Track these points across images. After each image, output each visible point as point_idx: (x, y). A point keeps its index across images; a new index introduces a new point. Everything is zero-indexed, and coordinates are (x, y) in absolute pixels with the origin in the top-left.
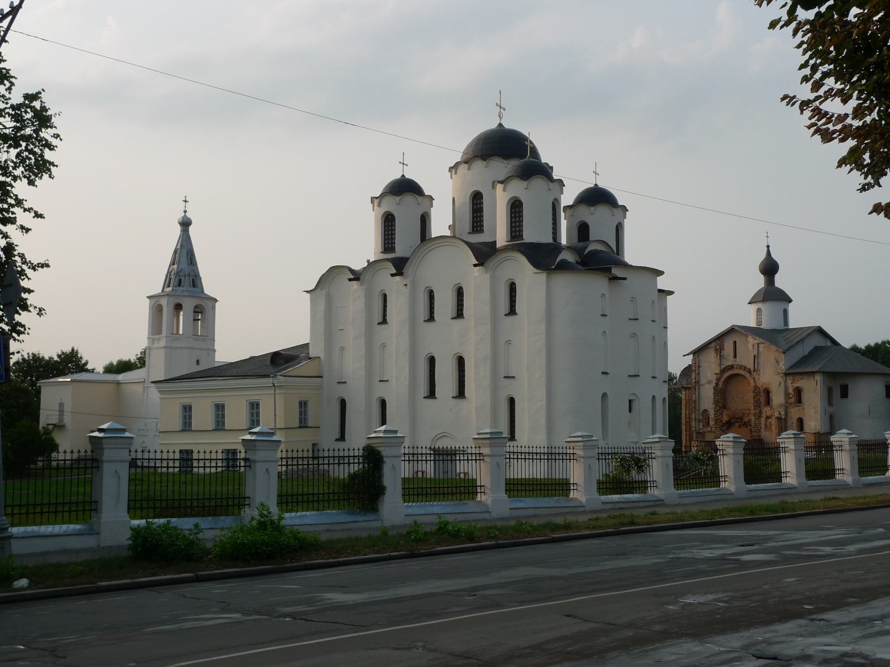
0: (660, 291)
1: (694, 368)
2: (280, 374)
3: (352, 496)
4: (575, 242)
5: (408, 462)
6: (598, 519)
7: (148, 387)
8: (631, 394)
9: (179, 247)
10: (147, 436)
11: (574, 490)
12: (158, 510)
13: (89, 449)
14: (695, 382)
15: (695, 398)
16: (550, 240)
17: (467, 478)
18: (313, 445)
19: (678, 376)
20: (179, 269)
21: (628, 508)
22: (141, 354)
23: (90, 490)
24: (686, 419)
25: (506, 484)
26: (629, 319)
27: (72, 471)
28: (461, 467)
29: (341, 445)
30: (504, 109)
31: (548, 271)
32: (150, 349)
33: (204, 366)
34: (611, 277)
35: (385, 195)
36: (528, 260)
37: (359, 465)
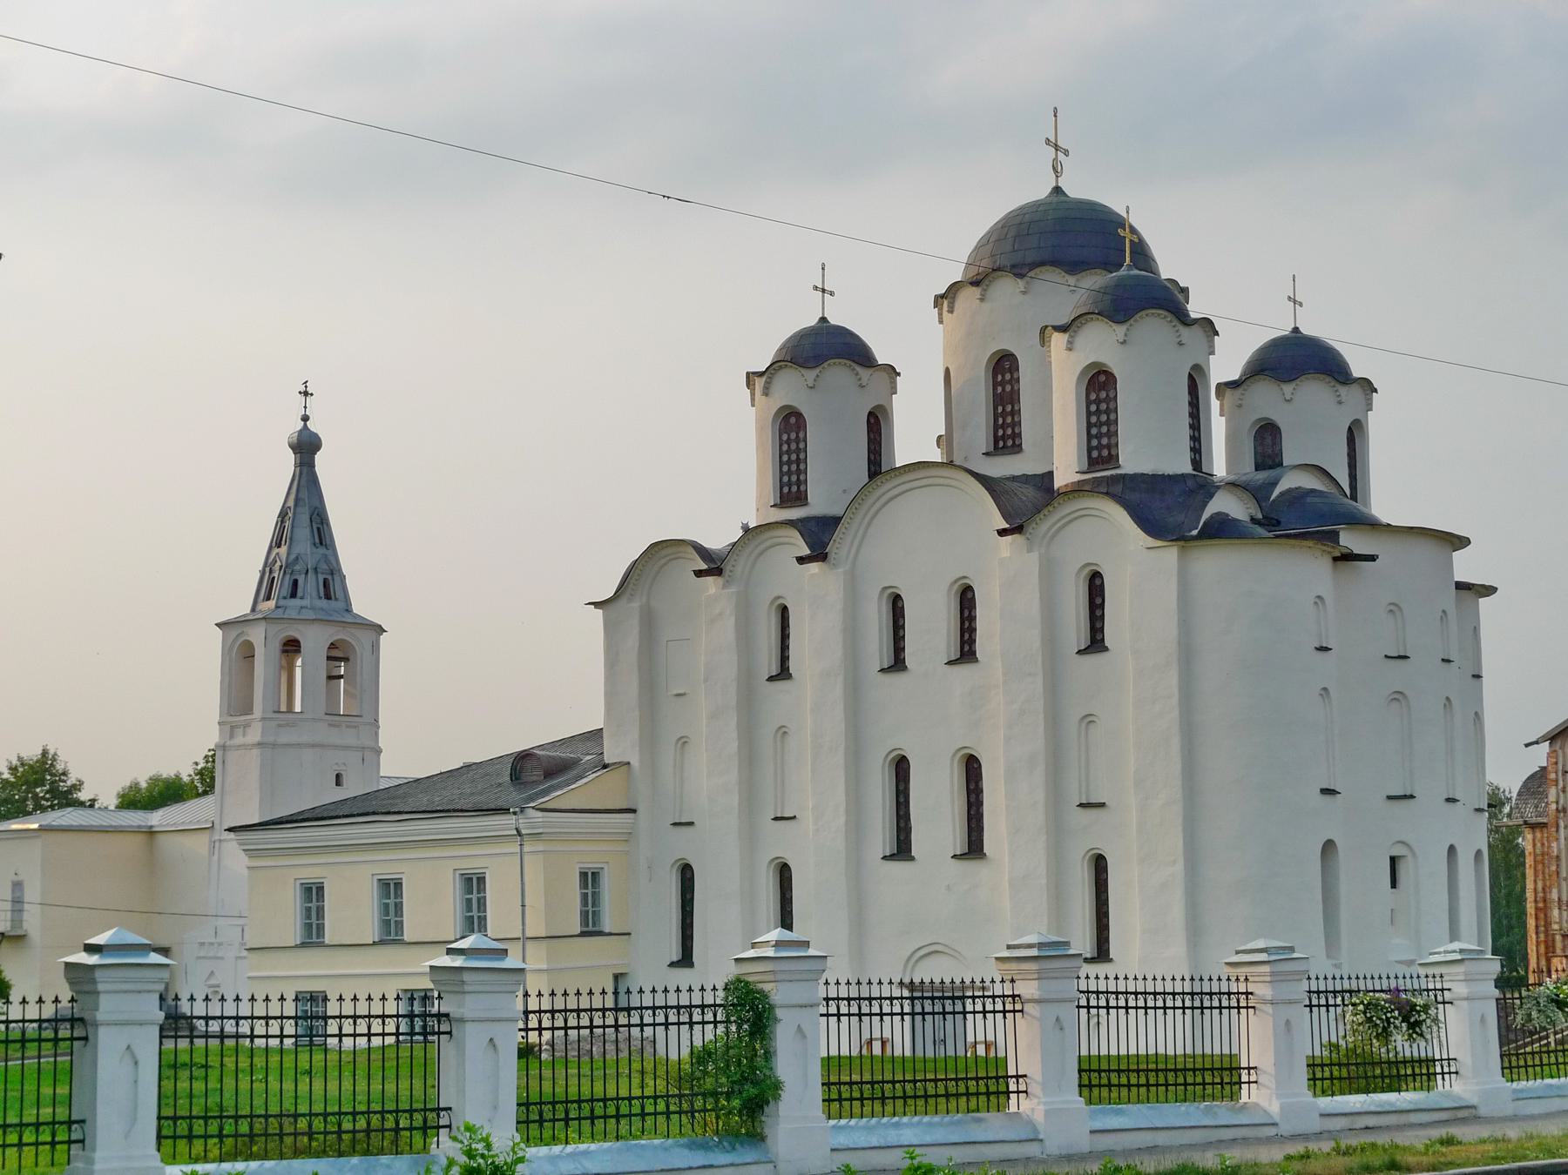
0: (1460, 586)
1: (1553, 776)
2: (532, 805)
3: (699, 1104)
4: (1248, 470)
5: (899, 1017)
6: (1308, 1157)
7: (220, 841)
8: (1393, 844)
9: (291, 503)
10: (222, 958)
11: (1018, 1092)
12: (229, 1142)
13: (66, 994)
14: (1557, 809)
15: (1559, 850)
16: (1187, 468)
17: (992, 1054)
18: (617, 978)
19: (1514, 795)
20: (292, 557)
21: (1388, 1128)
22: (207, 762)
23: (66, 1091)
24: (1536, 901)
25: (1080, 1071)
26: (1386, 656)
27: (23, 1047)
28: (978, 1029)
29: (683, 977)
30: (1066, 153)
31: (1182, 543)
32: (224, 750)
33: (351, 789)
34: (1338, 554)
35: (781, 367)
36: (1131, 516)
37: (715, 1027)
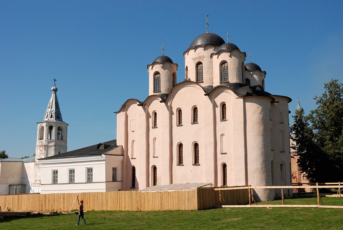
8: (282, 161)
35: (155, 63)
